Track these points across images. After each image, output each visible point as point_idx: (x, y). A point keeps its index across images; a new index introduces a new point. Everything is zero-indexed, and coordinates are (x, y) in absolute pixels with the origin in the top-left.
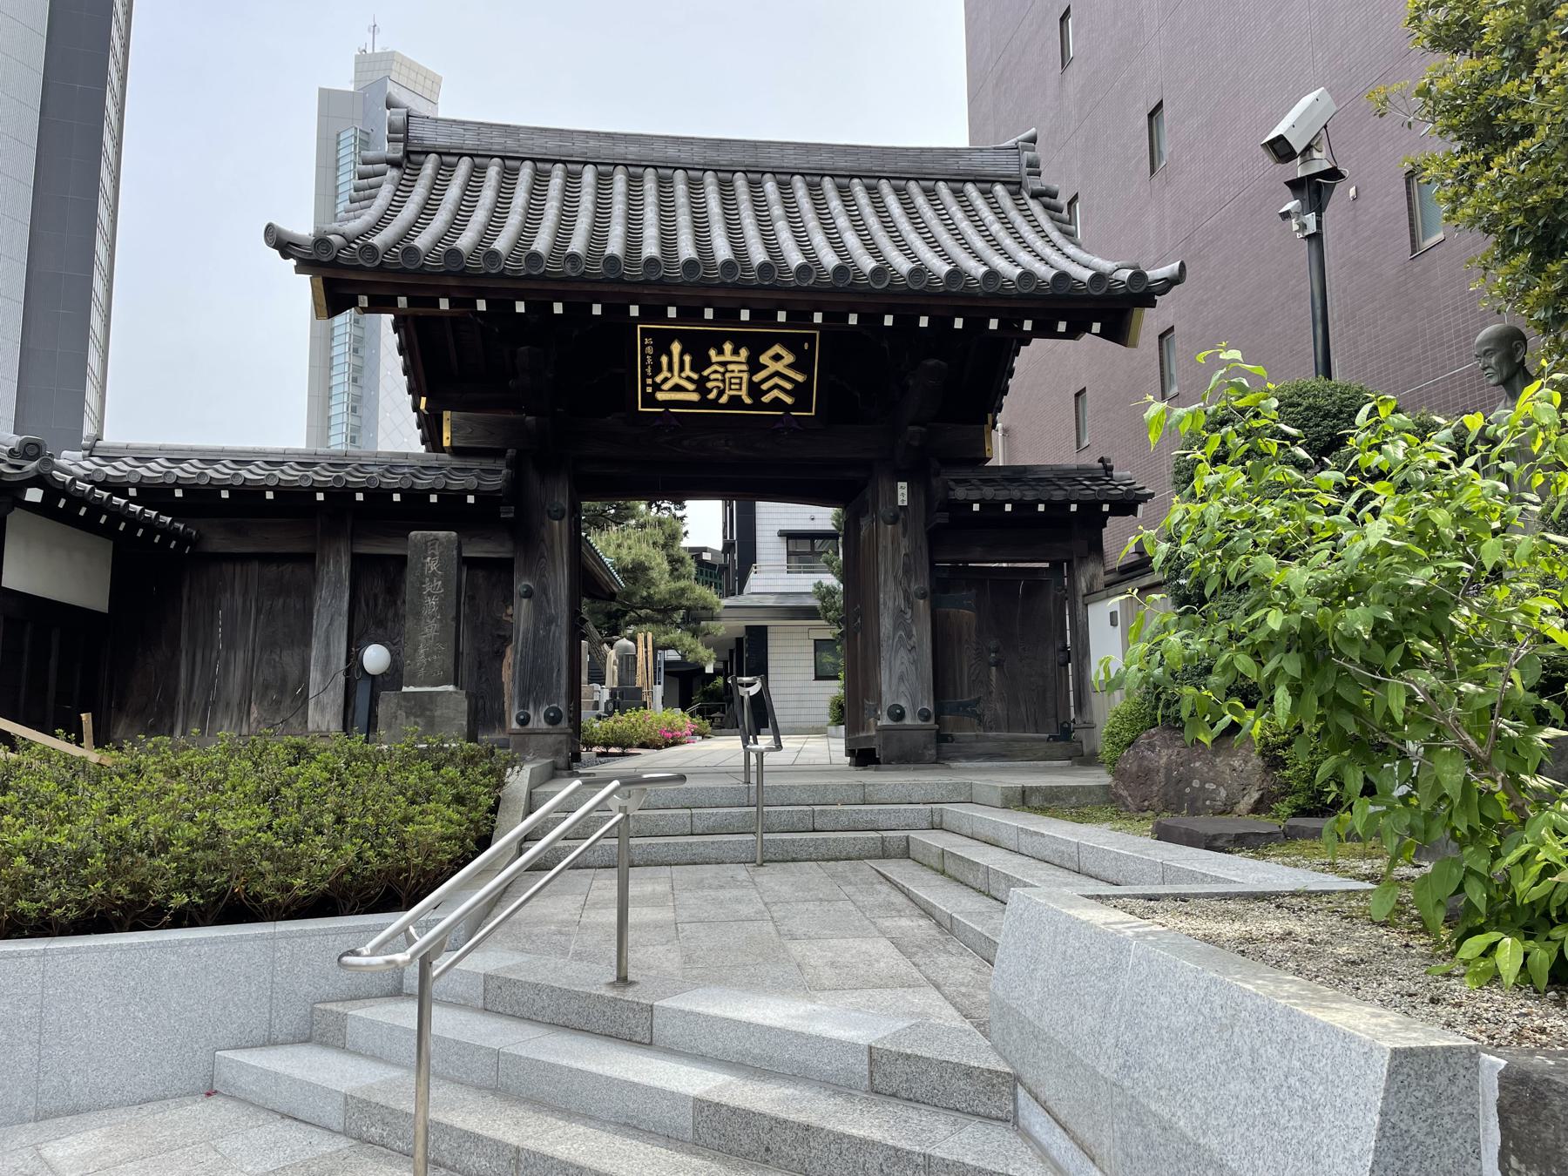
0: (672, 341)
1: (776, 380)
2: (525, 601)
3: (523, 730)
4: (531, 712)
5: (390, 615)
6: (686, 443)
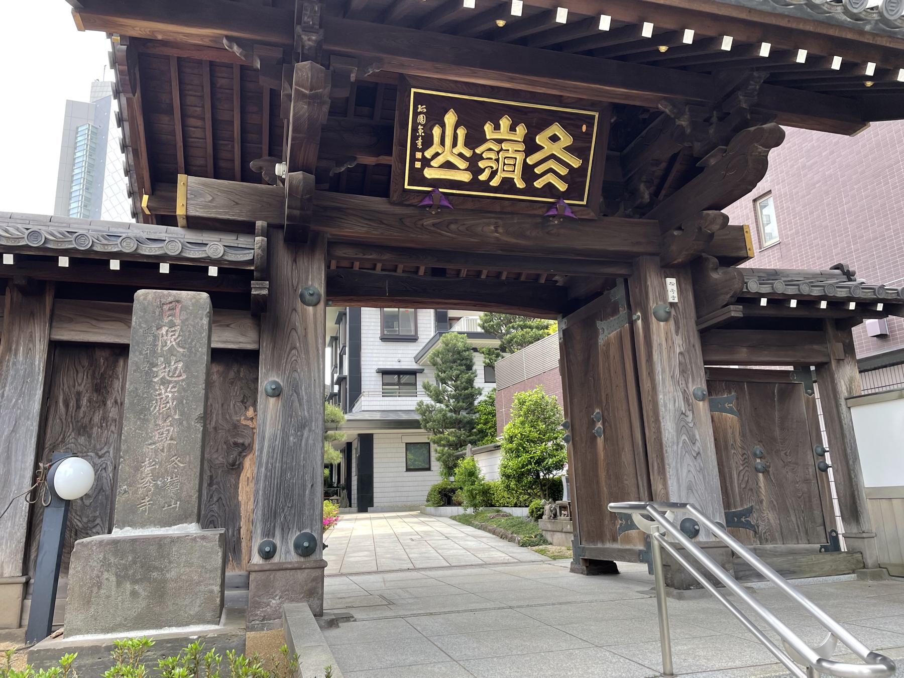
0: (446, 112)
1: (552, 164)
2: (272, 400)
3: (267, 564)
4: (277, 541)
5: (96, 419)
6: (453, 227)
